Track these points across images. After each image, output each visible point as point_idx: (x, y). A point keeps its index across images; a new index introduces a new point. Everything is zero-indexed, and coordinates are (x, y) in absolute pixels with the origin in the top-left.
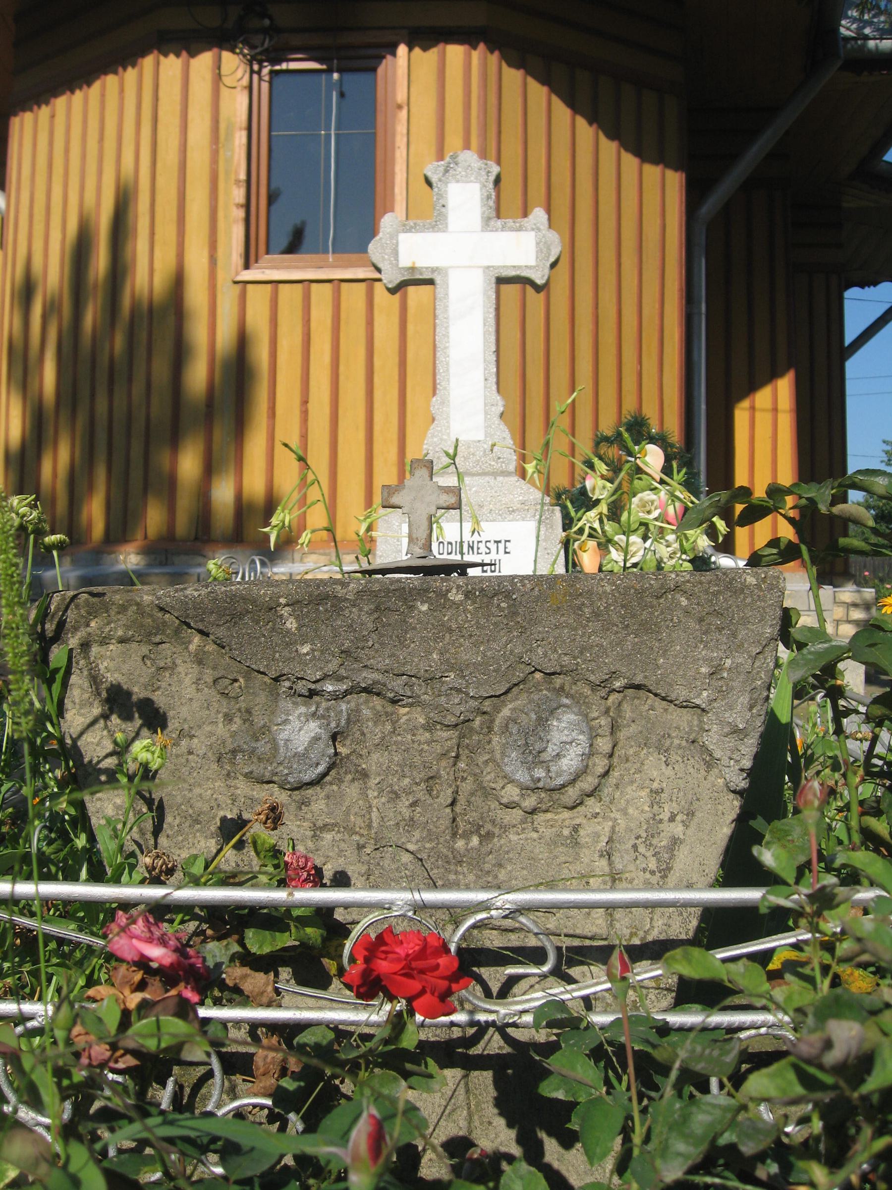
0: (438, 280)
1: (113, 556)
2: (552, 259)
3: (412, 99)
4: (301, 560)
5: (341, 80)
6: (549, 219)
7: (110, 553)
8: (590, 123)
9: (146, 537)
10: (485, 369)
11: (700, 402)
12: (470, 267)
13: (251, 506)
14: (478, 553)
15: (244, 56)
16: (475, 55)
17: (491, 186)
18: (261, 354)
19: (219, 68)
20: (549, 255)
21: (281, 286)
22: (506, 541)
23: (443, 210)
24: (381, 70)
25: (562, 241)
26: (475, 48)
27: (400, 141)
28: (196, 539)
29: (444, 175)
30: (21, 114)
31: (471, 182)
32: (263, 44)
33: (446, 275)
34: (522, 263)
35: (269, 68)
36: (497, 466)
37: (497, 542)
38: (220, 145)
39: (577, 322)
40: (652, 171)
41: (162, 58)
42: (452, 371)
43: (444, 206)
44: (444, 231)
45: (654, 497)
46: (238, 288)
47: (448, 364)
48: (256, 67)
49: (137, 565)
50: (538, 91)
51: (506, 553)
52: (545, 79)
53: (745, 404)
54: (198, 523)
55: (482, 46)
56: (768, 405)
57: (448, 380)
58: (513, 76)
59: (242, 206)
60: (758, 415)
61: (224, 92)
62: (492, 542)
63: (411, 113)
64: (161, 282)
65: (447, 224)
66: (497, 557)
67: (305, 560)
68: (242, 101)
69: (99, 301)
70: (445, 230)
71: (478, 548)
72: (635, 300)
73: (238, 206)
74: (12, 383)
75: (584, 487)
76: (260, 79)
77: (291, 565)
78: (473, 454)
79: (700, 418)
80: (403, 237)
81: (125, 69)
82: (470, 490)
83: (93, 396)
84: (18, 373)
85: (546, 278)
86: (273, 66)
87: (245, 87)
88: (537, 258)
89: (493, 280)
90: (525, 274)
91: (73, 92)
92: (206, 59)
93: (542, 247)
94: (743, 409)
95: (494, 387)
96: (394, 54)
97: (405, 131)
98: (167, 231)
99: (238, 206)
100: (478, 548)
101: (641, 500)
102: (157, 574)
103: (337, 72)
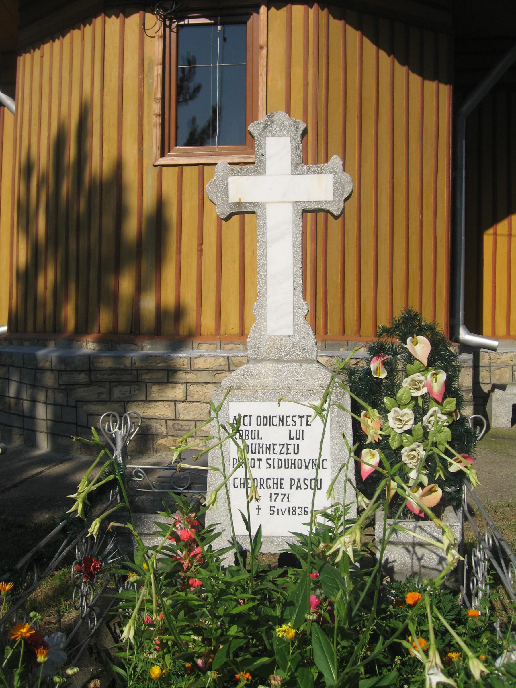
0: (258, 212)
1: (79, 343)
2: (346, 196)
3: (269, 43)
4: (198, 348)
5: (223, 31)
6: (344, 164)
7: (77, 341)
8: (389, 55)
9: (99, 332)
10: (294, 281)
11: (461, 235)
12: (282, 202)
13: (166, 312)
14: (287, 425)
15: (160, 16)
16: (312, 12)
17: (299, 139)
18: (172, 213)
19: (144, 25)
20: (343, 192)
21: (184, 167)
22: (308, 416)
23: (262, 158)
24: (249, 23)
25: (353, 180)
26: (311, 7)
27: (262, 71)
28: (131, 332)
29: (263, 130)
30: (24, 55)
31: (283, 136)
32: (171, 8)
33: (265, 208)
34: (323, 199)
35: (176, 23)
36: (302, 355)
37: (301, 417)
38: (145, 76)
39: (379, 188)
40: (430, 86)
41: (107, 18)
42: (269, 282)
43: (263, 155)
44: (263, 175)
45: (422, 378)
46: (156, 169)
47: (265, 277)
48: (168, 23)
49: (94, 349)
50: (354, 34)
51: (307, 425)
52: (357, 27)
53: (491, 231)
54: (132, 323)
55: (316, 5)
56: (506, 232)
57: (266, 289)
58: (337, 25)
59: (159, 115)
60: (499, 238)
61: (147, 40)
62: (297, 417)
63: (269, 51)
64: (107, 166)
65: (265, 168)
66: (301, 428)
67: (201, 348)
68: (158, 45)
69: (71, 177)
70: (264, 173)
71: (287, 421)
72: (418, 171)
73: (157, 115)
74: (20, 227)
75: (369, 369)
76: (171, 31)
77: (191, 351)
78: (285, 346)
79: (461, 246)
80: (231, 179)
81: (34, 50)
82: (281, 375)
83: (67, 238)
84: (24, 221)
85: (341, 210)
86: (179, 22)
87: (161, 37)
88: (334, 194)
89: (300, 212)
90: (324, 207)
91: (54, 41)
92: (135, 18)
93: (338, 186)
94: (489, 235)
95: (301, 295)
96: (258, 13)
97: (265, 64)
98: (111, 133)
99: (157, 115)
100: (287, 421)
101: (413, 380)
102: (105, 357)
103: (220, 25)
